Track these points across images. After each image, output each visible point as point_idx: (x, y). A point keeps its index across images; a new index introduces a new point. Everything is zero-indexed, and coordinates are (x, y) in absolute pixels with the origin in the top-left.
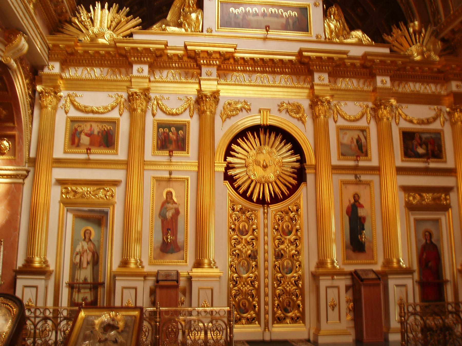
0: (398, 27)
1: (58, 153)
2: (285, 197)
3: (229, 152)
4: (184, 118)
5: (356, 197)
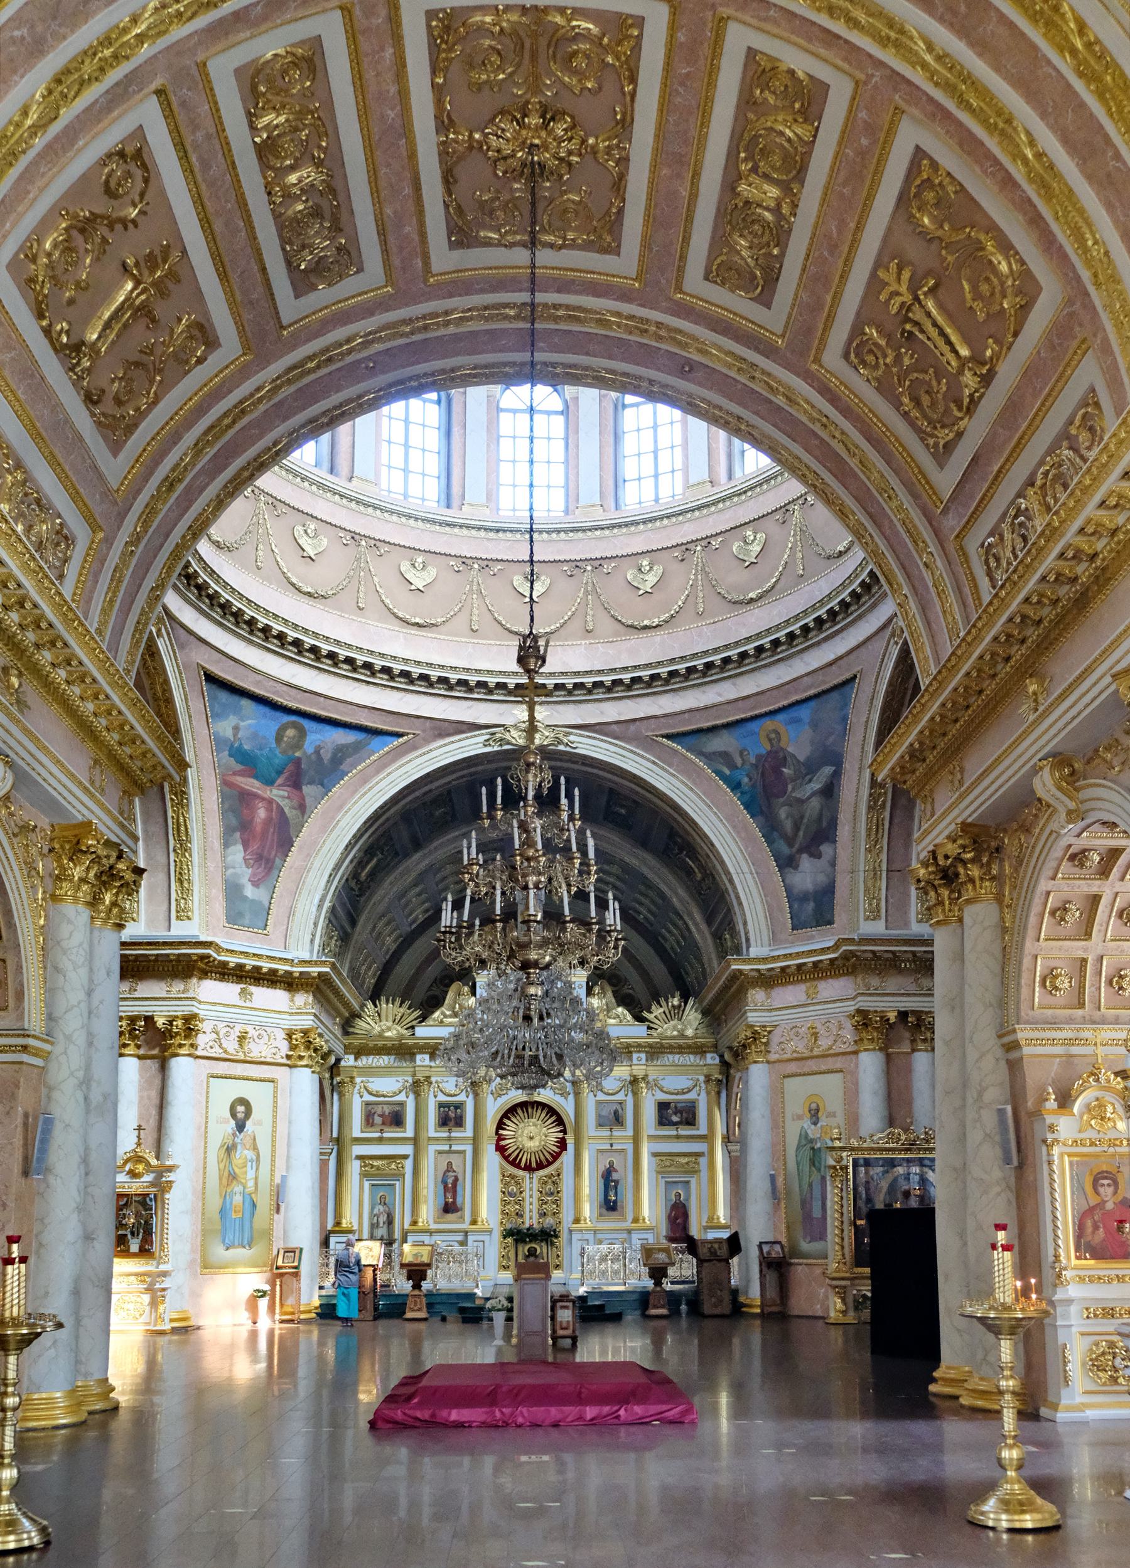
0: (659, 1003)
1: (357, 1132)
2: (549, 1164)
3: (500, 1125)
4: (462, 1097)
5: (611, 1164)
